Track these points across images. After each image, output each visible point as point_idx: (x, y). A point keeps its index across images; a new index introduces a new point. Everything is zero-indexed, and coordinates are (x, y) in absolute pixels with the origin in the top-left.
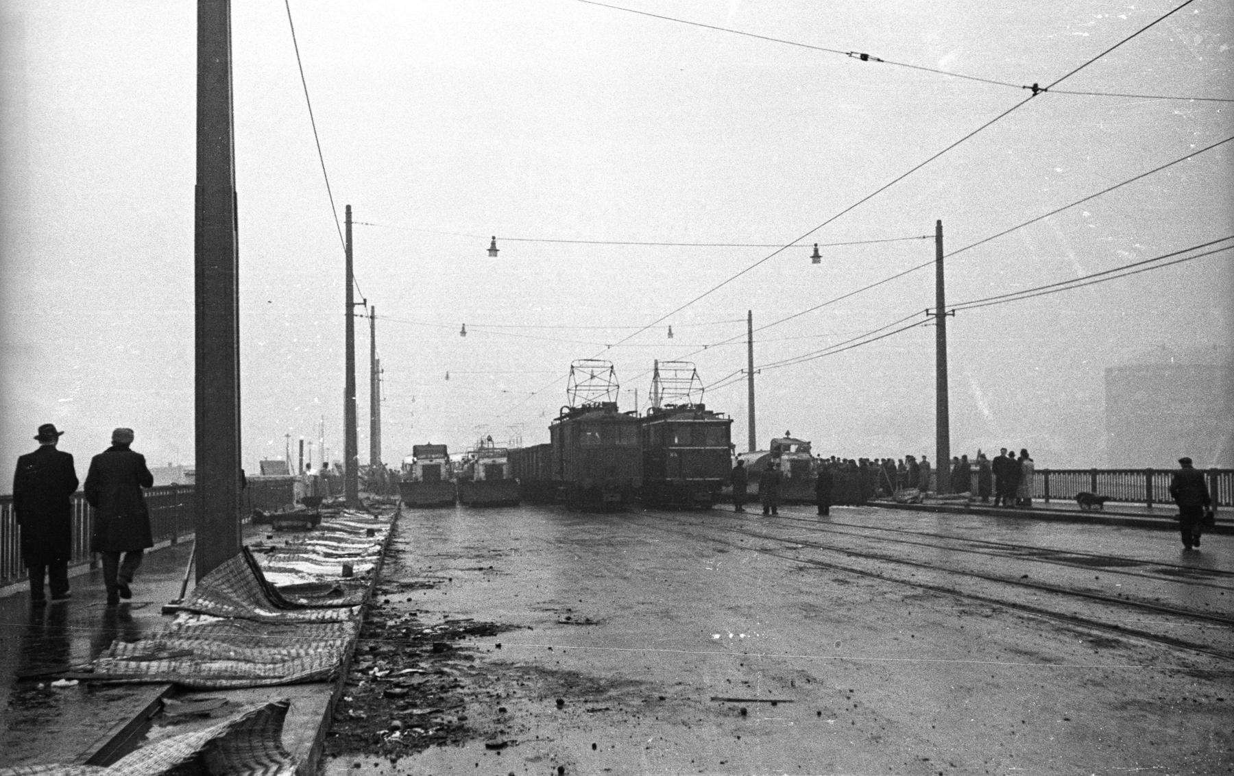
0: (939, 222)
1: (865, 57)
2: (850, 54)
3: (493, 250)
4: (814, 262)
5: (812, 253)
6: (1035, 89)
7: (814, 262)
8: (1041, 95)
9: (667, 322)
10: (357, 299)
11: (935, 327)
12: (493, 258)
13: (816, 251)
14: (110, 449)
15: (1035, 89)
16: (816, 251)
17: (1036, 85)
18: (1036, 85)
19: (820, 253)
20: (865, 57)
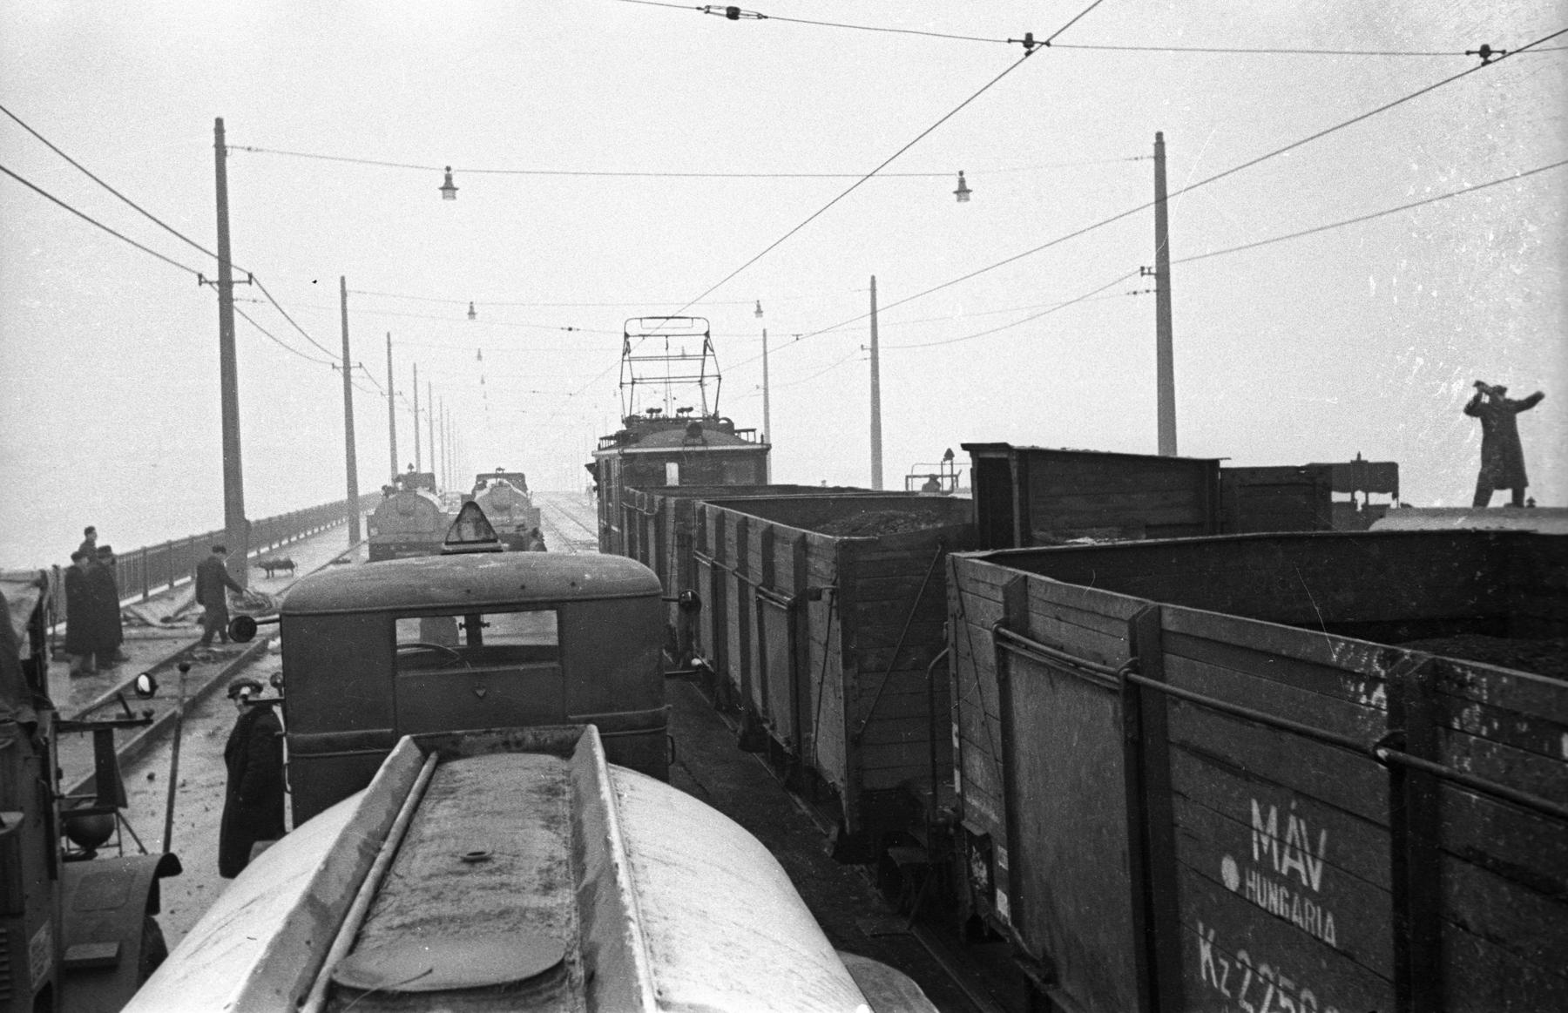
0: (1159, 136)
2: (708, 10)
6: (1029, 42)
8: (1040, 53)
10: (395, 390)
12: (450, 202)
15: (1029, 42)
17: (1029, 36)
18: (1029, 36)
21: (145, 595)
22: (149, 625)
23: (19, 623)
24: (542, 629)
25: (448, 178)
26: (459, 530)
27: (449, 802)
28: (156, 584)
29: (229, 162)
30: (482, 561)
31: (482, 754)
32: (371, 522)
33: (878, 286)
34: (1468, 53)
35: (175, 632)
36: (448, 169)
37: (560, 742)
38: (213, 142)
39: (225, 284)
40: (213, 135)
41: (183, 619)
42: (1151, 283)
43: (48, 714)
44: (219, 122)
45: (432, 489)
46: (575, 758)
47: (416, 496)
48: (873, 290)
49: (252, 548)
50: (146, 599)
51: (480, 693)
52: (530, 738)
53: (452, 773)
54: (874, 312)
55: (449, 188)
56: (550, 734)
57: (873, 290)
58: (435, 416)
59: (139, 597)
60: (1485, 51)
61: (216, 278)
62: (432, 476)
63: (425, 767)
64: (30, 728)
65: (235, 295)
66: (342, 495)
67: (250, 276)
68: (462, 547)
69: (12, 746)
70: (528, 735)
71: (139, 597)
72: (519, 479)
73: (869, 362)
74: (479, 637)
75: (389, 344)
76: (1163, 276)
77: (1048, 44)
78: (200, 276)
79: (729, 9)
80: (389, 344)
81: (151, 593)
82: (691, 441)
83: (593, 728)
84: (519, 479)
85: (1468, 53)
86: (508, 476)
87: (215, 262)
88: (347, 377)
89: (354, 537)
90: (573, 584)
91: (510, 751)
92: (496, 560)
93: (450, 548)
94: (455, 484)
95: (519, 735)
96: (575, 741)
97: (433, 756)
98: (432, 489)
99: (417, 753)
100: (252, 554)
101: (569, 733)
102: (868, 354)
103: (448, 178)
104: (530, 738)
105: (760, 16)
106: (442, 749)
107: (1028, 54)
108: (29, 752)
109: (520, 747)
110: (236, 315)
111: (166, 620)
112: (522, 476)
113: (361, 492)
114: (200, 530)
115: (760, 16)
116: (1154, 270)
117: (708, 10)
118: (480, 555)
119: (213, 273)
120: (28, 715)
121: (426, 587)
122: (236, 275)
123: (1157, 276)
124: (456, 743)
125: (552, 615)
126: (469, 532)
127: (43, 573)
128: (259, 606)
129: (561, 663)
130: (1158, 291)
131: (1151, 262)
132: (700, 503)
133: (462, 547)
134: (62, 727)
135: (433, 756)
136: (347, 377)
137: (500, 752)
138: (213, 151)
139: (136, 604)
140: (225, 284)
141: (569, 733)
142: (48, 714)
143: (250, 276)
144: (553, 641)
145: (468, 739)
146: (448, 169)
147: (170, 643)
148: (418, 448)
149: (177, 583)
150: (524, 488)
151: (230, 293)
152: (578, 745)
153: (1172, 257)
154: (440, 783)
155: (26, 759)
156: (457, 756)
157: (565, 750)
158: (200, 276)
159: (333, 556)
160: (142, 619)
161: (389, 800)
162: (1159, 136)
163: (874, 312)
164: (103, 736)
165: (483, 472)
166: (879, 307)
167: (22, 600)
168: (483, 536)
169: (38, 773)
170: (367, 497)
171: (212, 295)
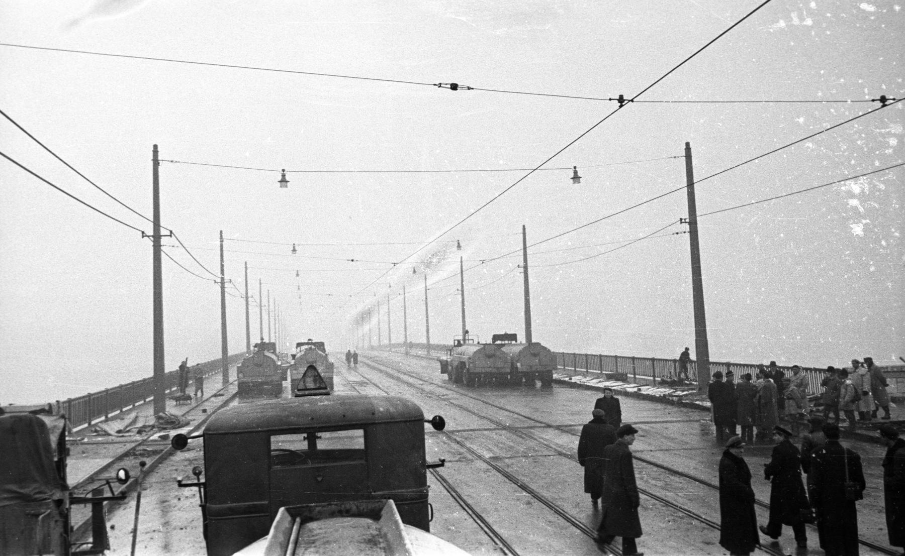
0: (688, 144)
1: (454, 87)
2: (440, 85)
3: (284, 181)
4: (574, 183)
5: (572, 175)
6: (621, 100)
7: (574, 183)
8: (628, 107)
9: (568, 160)
10: (249, 295)
11: (688, 235)
12: (284, 189)
13: (576, 172)
14: (586, 471)
15: (621, 100)
16: (576, 172)
17: (621, 97)
18: (621, 97)
19: (579, 174)
20: (454, 87)
21: (106, 417)
22: (110, 435)
23: (54, 439)
24: (355, 439)
25: (284, 176)
26: (304, 382)
27: (312, 549)
28: (112, 410)
29: (160, 169)
30: (320, 401)
31: (326, 518)
32: (240, 370)
33: (527, 231)
34: (873, 100)
35: (123, 439)
36: (283, 170)
37: (372, 510)
38: (152, 158)
39: (157, 237)
40: (152, 153)
41: (128, 431)
42: (687, 227)
43: (67, 493)
44: (155, 147)
45: (274, 353)
46: (382, 520)
47: (265, 356)
48: (524, 234)
49: (167, 388)
50: (107, 420)
51: (319, 479)
52: (354, 508)
53: (310, 531)
54: (525, 248)
55: (284, 181)
56: (364, 505)
57: (524, 234)
58: (272, 307)
59: (103, 418)
60: (883, 99)
61: (151, 233)
62: (274, 345)
63: (295, 527)
64: (59, 503)
65: (162, 243)
66: (219, 356)
67: (171, 232)
68: (307, 392)
69: (49, 514)
70: (352, 505)
71: (103, 418)
72: (321, 345)
73: (523, 275)
74: (315, 445)
75: (246, 268)
76: (693, 223)
77: (632, 101)
78: (143, 233)
79: (452, 85)
80: (246, 268)
81: (110, 416)
82: (781, 472)
83: (392, 501)
84: (321, 345)
85: (873, 100)
86: (315, 344)
87: (152, 225)
88: (223, 288)
89: (226, 381)
90: (373, 414)
91: (343, 516)
92: (327, 400)
93: (301, 393)
94: (288, 348)
95: (348, 507)
96: (381, 510)
97: (298, 520)
98: (274, 353)
99: (289, 518)
100: (167, 391)
101: (377, 505)
102: (522, 270)
103: (284, 176)
104: (354, 508)
105: (469, 88)
106: (303, 515)
107: (621, 106)
108: (57, 518)
109: (348, 513)
110: (163, 255)
111: (119, 432)
112: (322, 344)
113: (231, 353)
114: (138, 378)
115: (469, 88)
116: (688, 220)
117: (440, 85)
118: (318, 397)
119: (150, 231)
120: (58, 495)
121: (288, 416)
122: (163, 232)
123: (690, 223)
124: (310, 512)
125: (360, 432)
126: (310, 384)
127: (50, 405)
128: (173, 423)
129: (366, 461)
130: (690, 232)
131: (686, 215)
132: (814, 510)
133: (307, 392)
134: (75, 501)
135: (298, 520)
136: (223, 288)
137: (336, 516)
138: (152, 163)
139: (101, 422)
140: (157, 237)
141: (377, 505)
142: (67, 493)
143: (171, 232)
144: (363, 447)
145: (318, 509)
146: (283, 170)
147: (122, 445)
148: (261, 328)
149: (124, 410)
150: (324, 351)
151: (160, 242)
152: (383, 512)
153: (698, 213)
154: (304, 538)
155: (56, 521)
156: (312, 519)
157: (376, 515)
158: (143, 233)
159: (215, 392)
160: (105, 431)
161: (279, 549)
162: (688, 144)
163: (525, 248)
164: (97, 504)
165: (299, 341)
166: (528, 245)
167: (55, 427)
168: (318, 385)
169: (62, 530)
170: (236, 356)
171: (149, 243)
